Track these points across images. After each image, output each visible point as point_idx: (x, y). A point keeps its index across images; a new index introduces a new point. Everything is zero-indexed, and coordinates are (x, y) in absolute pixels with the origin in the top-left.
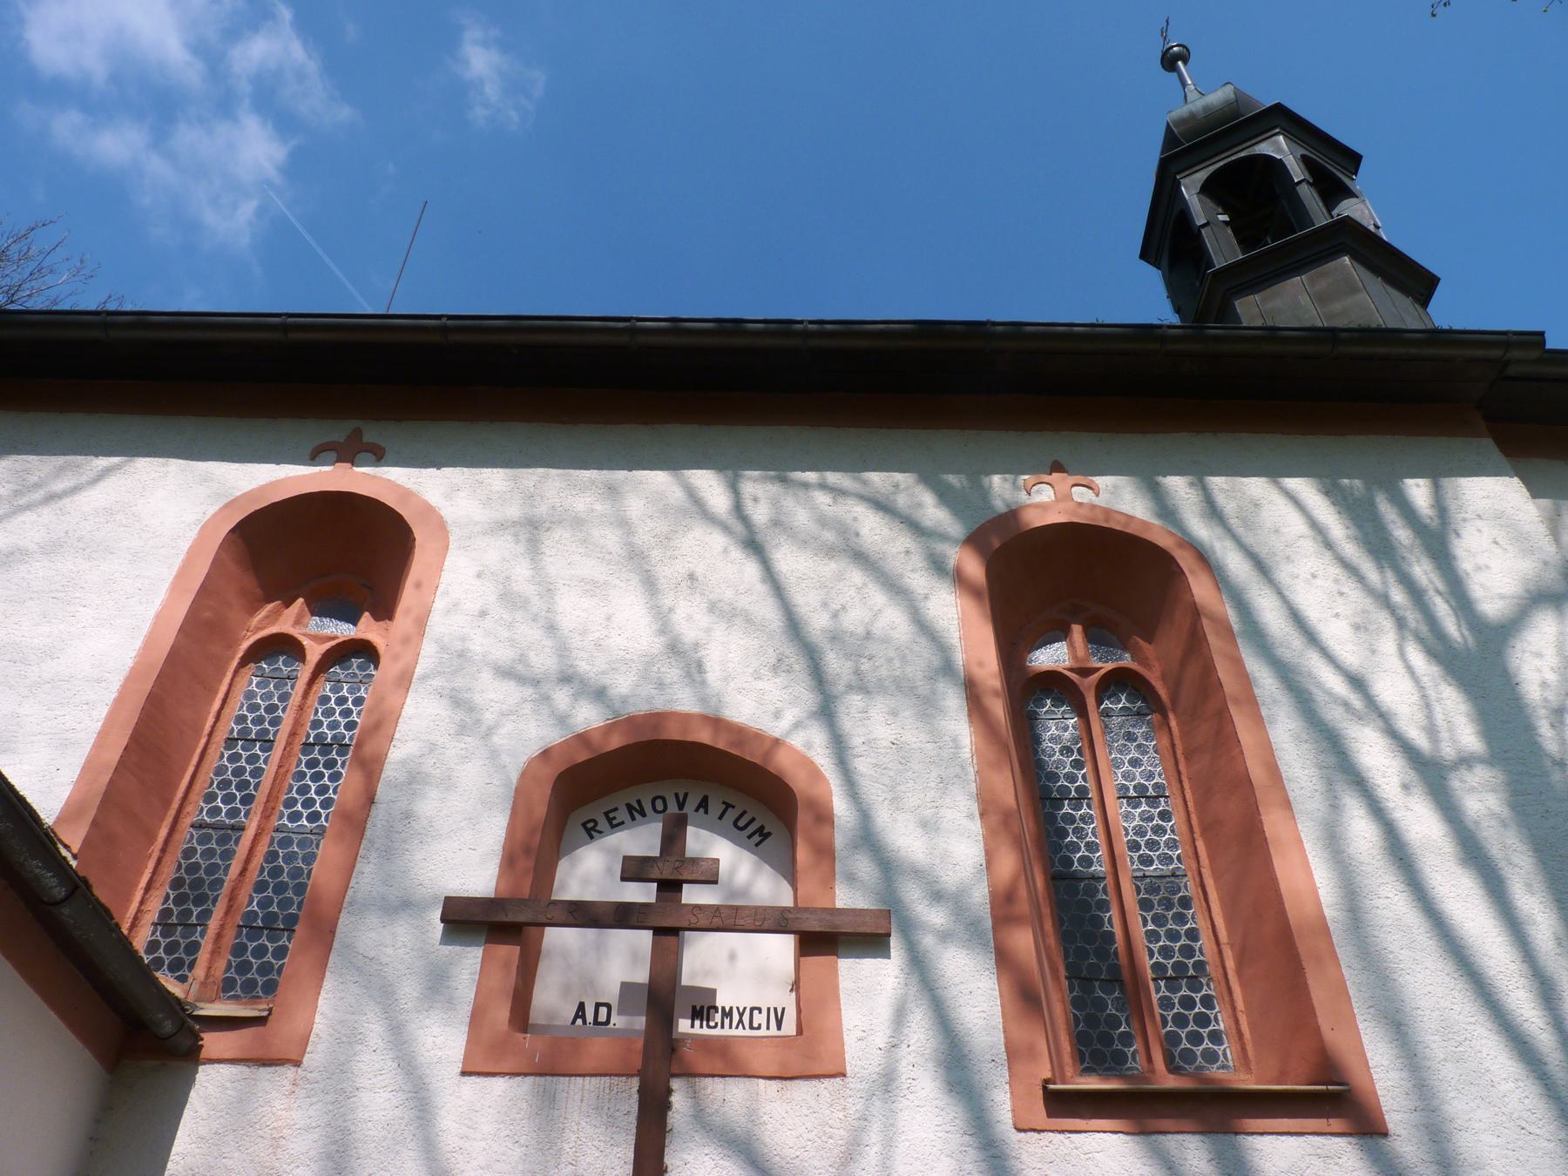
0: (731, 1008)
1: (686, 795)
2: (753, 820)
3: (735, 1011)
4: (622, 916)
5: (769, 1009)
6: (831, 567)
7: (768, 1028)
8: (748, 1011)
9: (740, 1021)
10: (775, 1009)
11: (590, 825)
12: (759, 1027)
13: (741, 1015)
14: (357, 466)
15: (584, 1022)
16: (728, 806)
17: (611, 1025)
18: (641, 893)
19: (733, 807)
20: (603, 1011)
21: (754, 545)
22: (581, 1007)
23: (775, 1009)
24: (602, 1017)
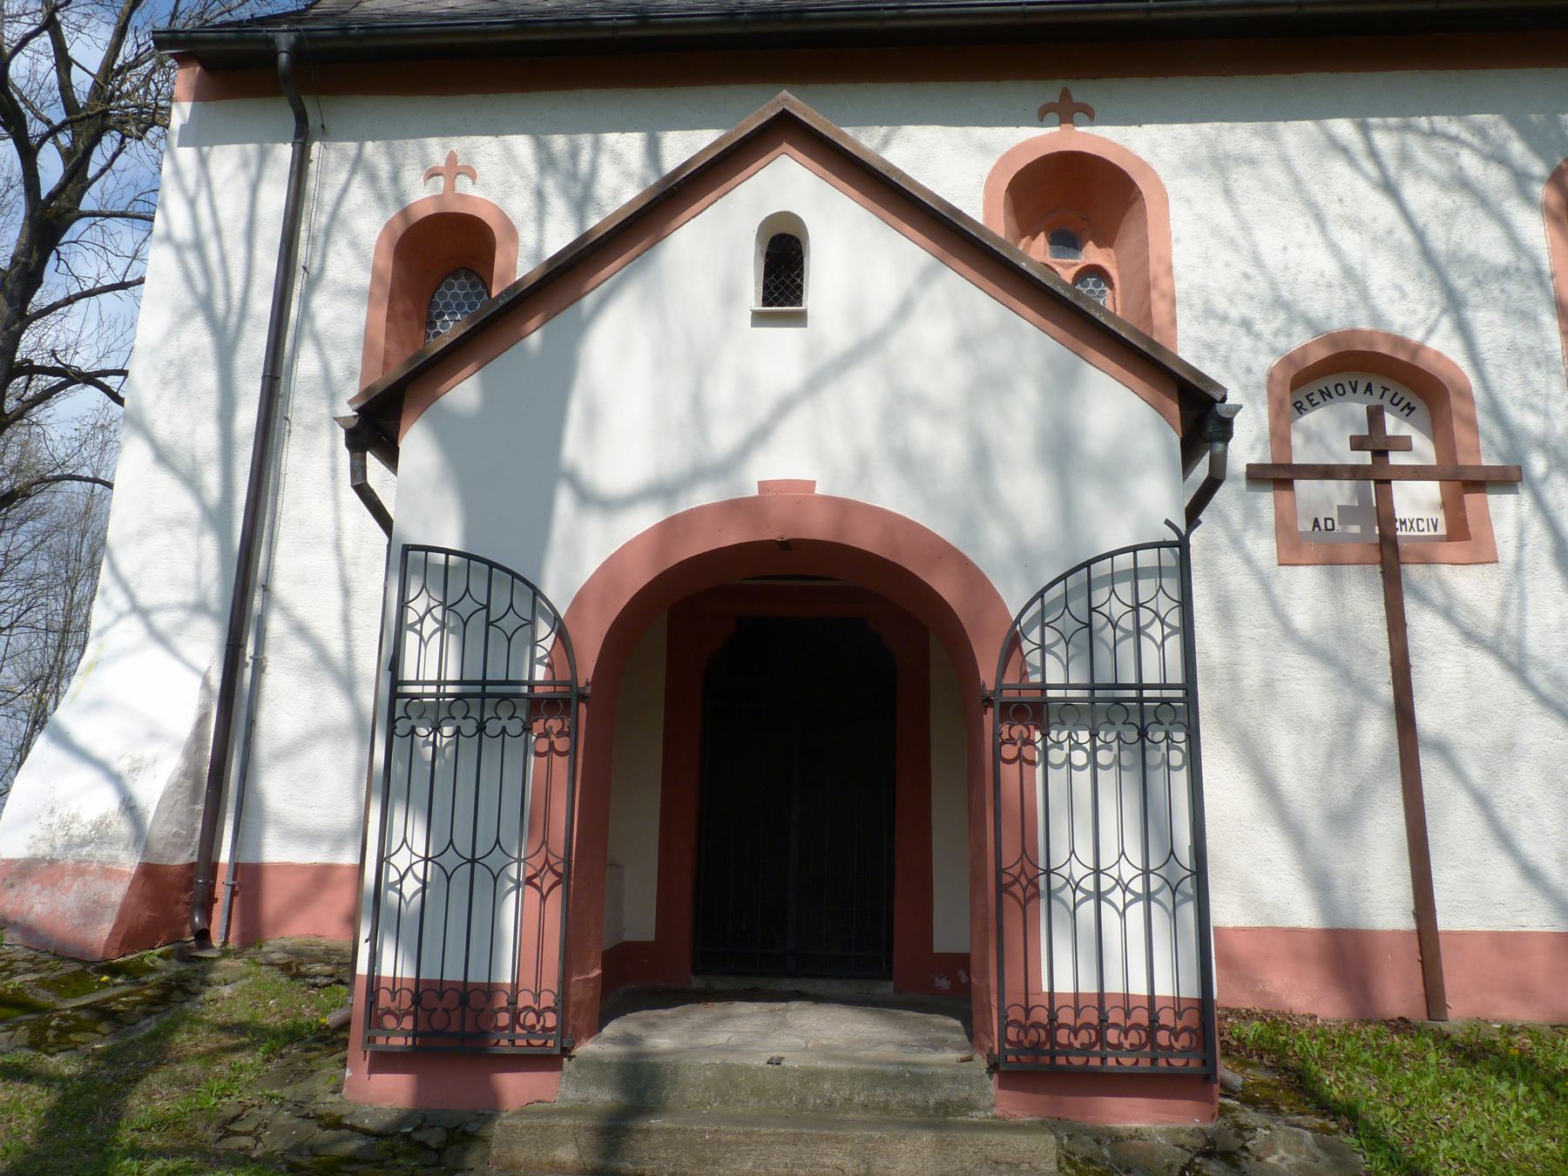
0: (1405, 520)
1: (1356, 382)
2: (1402, 399)
3: (1407, 521)
4: (1354, 472)
5: (1428, 520)
6: (1447, 202)
7: (1429, 530)
8: (1415, 521)
9: (1412, 527)
10: (1432, 519)
11: (1298, 405)
12: (1423, 530)
13: (1412, 523)
14: (1077, 126)
15: (1320, 529)
16: (1385, 389)
17: (1335, 531)
18: (1365, 458)
19: (1388, 390)
20: (1329, 522)
21: (1390, 189)
22: (1316, 521)
23: (1432, 519)
24: (1330, 526)
